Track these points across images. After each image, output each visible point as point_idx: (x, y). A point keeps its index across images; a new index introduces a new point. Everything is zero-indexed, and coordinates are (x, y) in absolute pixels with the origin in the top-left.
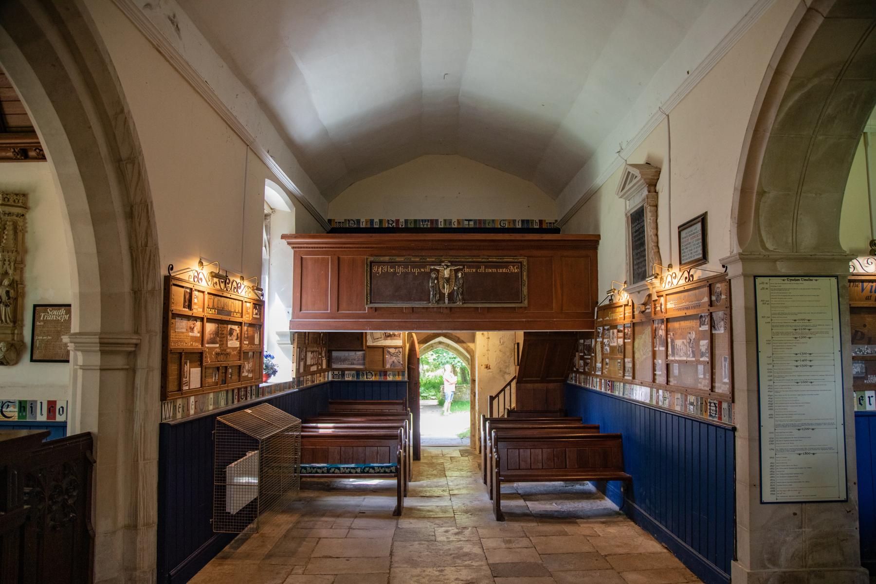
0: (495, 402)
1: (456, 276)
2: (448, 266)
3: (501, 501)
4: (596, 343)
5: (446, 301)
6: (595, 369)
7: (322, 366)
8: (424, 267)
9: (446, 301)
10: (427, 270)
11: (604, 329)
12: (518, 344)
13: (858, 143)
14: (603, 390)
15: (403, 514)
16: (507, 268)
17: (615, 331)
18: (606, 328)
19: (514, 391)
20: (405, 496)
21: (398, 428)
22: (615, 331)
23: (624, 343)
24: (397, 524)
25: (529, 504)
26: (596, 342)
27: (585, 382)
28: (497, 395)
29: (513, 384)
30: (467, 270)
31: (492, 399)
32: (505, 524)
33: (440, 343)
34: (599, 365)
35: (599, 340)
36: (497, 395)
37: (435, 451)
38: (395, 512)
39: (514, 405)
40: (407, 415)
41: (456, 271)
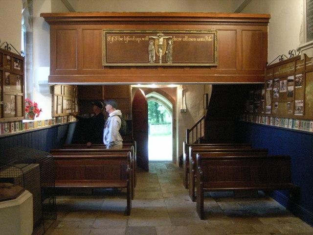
0: (191, 133)
1: (168, 44)
2: (162, 36)
3: (204, 203)
4: (266, 93)
5: (161, 61)
6: (265, 110)
7: (75, 109)
8: (144, 37)
9: (161, 61)
10: (147, 39)
11: (274, 81)
12: (207, 95)
13: (212, 95)
14: (271, 124)
15: (131, 214)
16: (203, 37)
17: (285, 81)
18: (276, 80)
19: (203, 126)
20: (133, 199)
21: (128, 151)
22: (285, 81)
23: (295, 89)
24: (127, 222)
25: (220, 204)
26: (266, 91)
27: (255, 119)
28: (192, 129)
29: (203, 122)
30: (175, 39)
31: (189, 131)
32: (207, 222)
33: (152, 97)
34: (269, 107)
35: (269, 89)
36: (192, 129)
37: (153, 164)
38: (125, 211)
39: (203, 135)
40: (132, 142)
41: (168, 40)
